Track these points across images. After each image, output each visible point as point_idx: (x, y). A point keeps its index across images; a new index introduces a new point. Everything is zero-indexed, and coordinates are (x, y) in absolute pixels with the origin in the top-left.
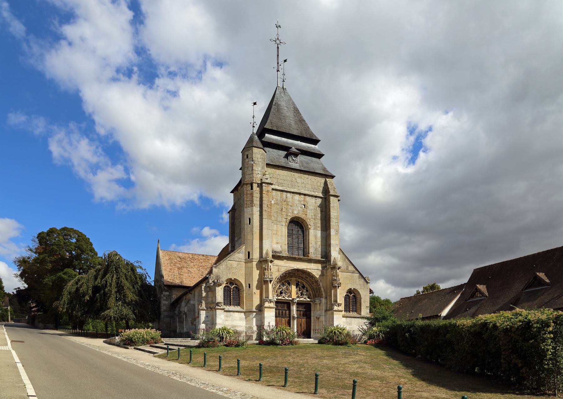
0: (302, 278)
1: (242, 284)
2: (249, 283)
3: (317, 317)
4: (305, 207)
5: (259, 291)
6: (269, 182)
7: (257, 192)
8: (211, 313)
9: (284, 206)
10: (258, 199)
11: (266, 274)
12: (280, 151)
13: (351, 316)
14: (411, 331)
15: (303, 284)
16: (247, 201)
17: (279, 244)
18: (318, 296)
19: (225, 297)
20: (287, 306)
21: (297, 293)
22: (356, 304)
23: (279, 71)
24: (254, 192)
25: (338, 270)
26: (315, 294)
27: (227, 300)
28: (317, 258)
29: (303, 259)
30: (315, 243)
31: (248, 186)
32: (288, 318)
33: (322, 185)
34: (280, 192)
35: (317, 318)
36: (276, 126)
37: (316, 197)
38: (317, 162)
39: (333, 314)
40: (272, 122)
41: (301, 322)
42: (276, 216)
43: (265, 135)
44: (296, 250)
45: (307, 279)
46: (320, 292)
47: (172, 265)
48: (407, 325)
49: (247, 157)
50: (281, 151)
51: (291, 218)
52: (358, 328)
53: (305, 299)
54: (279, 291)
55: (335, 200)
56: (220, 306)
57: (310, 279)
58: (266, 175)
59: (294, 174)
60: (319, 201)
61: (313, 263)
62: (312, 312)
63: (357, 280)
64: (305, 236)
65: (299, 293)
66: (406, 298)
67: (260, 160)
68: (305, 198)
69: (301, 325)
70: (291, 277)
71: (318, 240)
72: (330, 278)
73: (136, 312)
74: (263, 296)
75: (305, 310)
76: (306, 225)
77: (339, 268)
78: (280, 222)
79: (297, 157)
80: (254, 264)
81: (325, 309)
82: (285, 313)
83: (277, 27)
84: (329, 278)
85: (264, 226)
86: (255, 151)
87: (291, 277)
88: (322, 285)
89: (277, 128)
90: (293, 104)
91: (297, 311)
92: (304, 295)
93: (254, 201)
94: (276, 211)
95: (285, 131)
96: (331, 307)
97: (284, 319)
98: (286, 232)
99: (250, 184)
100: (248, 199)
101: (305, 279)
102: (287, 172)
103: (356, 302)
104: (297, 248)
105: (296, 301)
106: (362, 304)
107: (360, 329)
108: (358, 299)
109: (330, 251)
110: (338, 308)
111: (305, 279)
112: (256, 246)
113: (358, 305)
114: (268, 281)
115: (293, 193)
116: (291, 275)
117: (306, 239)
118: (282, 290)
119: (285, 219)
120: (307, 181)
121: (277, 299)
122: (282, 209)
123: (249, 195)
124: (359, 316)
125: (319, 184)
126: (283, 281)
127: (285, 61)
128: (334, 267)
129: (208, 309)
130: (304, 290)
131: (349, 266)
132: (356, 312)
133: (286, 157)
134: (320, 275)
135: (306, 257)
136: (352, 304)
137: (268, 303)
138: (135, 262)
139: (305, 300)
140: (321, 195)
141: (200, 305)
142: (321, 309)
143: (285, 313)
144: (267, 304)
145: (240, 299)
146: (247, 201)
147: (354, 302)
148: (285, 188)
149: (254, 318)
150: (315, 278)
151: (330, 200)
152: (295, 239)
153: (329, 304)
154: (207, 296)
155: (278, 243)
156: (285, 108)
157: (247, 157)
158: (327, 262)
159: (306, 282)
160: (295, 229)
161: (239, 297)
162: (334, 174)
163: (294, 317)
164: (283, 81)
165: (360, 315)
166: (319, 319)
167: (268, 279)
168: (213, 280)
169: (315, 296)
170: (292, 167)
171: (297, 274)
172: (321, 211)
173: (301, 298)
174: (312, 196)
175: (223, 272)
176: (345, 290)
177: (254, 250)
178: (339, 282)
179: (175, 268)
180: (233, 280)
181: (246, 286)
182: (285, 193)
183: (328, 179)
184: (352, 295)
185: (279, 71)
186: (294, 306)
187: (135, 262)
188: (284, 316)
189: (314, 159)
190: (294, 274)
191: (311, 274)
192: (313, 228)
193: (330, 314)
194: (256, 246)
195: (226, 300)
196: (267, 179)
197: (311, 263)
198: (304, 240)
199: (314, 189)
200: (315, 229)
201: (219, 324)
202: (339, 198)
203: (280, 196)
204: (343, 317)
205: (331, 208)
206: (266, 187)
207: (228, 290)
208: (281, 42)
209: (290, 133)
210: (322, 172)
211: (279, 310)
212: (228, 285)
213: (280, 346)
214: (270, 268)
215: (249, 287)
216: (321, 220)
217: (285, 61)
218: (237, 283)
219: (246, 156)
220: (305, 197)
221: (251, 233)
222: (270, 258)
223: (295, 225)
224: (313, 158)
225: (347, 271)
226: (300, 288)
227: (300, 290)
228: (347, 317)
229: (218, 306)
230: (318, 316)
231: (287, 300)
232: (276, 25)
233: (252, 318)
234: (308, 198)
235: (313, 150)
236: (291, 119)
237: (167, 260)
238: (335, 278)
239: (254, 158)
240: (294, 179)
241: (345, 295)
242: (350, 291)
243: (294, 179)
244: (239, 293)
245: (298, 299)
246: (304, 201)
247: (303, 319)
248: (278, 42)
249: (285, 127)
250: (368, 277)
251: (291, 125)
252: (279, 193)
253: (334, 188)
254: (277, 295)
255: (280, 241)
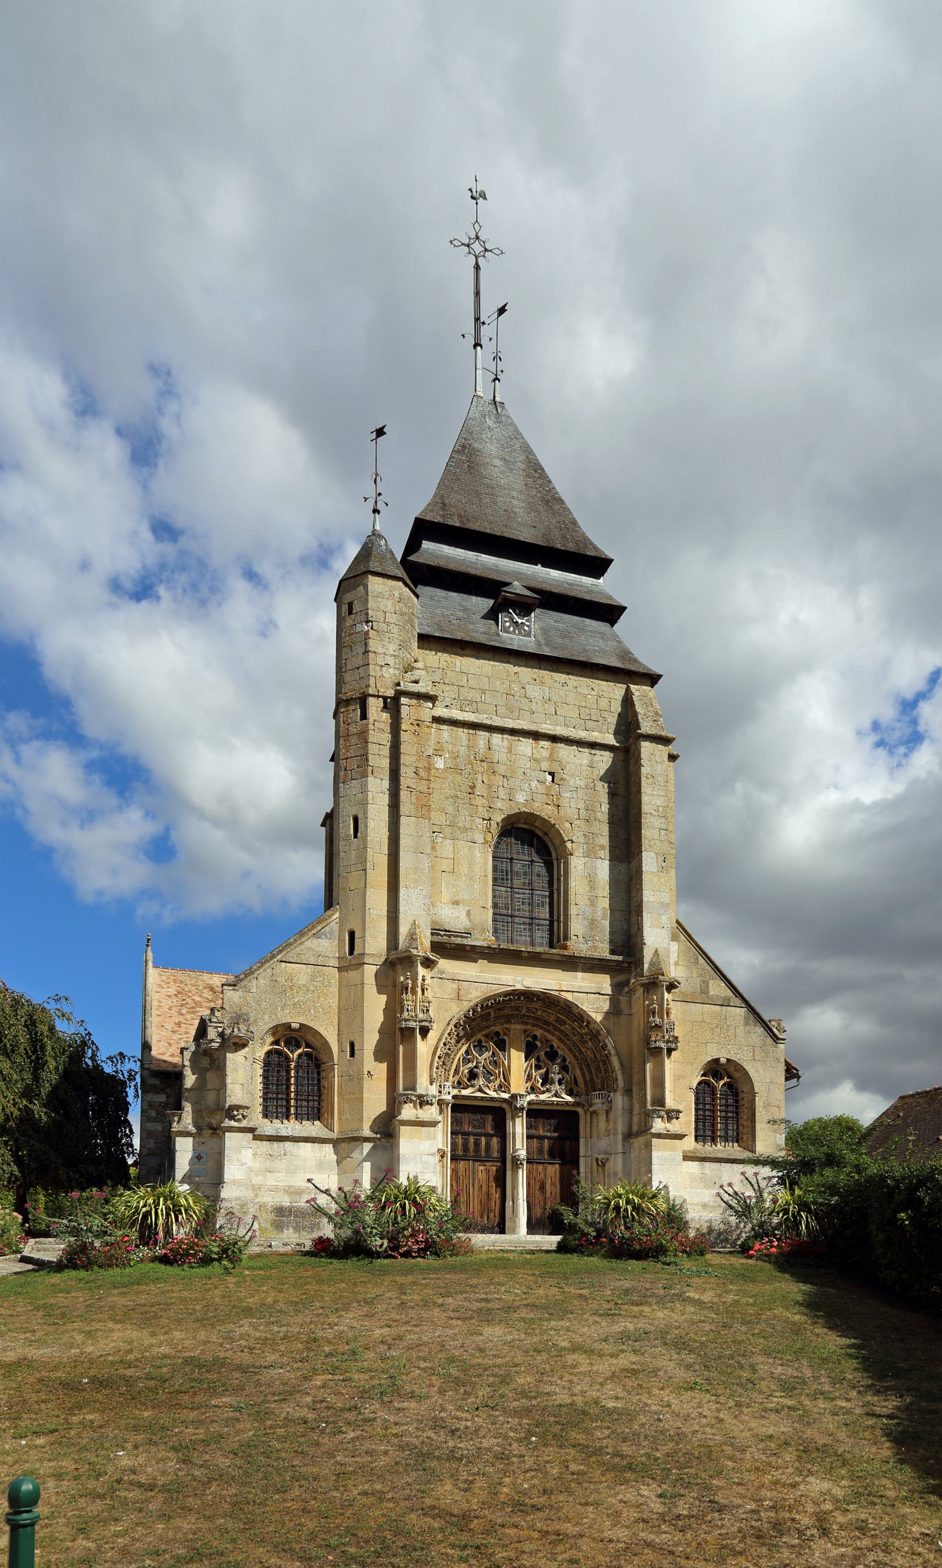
0: (547, 1023)
1: (326, 1043)
2: (352, 1038)
3: (597, 1159)
4: (553, 781)
5: (384, 1066)
6: (423, 690)
7: (382, 726)
8: (213, 1142)
9: (479, 776)
10: (386, 751)
11: (408, 1004)
12: (473, 597)
13: (720, 1155)
14: (921, 1201)
15: (552, 1047)
16: (346, 759)
17: (461, 905)
18: (603, 1085)
19: (267, 1088)
20: (493, 1120)
21: (529, 1078)
22: (737, 1113)
23: (481, 347)
24: (371, 727)
25: (669, 991)
26: (592, 1079)
27: (277, 1099)
28: (596, 955)
29: (544, 957)
30: (588, 903)
31: (352, 707)
32: (499, 1164)
33: (617, 707)
34: (466, 731)
35: (598, 1164)
36: (460, 516)
37: (593, 745)
38: (598, 633)
39: (648, 1146)
40: (446, 501)
41: (545, 1175)
42: (450, 809)
43: (421, 544)
44: (525, 929)
45: (563, 1028)
46: (606, 1071)
47: (184, 1011)
48: (903, 1178)
49: (350, 613)
50: (474, 599)
51: (503, 816)
52: (718, 1194)
53: (556, 1095)
54: (465, 1070)
55: (658, 753)
56: (239, 1120)
57: (573, 1028)
58: (415, 672)
59: (517, 669)
60: (604, 760)
61: (582, 971)
62: (582, 1141)
63: (741, 1031)
64: (555, 881)
65: (537, 1075)
66: (918, 1094)
67: (391, 618)
68: (552, 749)
69: (542, 1187)
70: (509, 1019)
71: (601, 893)
72: (642, 1023)
73: (23, 1156)
74: (398, 1082)
75: (556, 1134)
76: (557, 842)
77: (671, 987)
78: (465, 830)
79: (529, 614)
80: (370, 971)
81: (626, 1130)
82: (488, 1145)
83: (473, 197)
84: (638, 1021)
85: (401, 842)
86: (376, 586)
87: (509, 1022)
88: (616, 1048)
89: (461, 521)
90: (527, 450)
91: (528, 1137)
92: (552, 1083)
93: (370, 757)
94: (452, 793)
95: (488, 531)
96: (643, 1124)
97: (482, 1168)
98: (486, 863)
99: (358, 701)
100: (352, 753)
101: (555, 1028)
102: (492, 663)
103: (737, 1108)
104: (527, 921)
105: (523, 1102)
106: (757, 1113)
107: (726, 1197)
108: (743, 1095)
109: (640, 929)
110: (668, 1125)
111: (555, 1028)
112: (375, 912)
113: (745, 1117)
114: (413, 1029)
115: (513, 732)
116: (507, 1012)
117: (559, 890)
118: (476, 1067)
119: (484, 819)
120: (562, 693)
121: (454, 1097)
122: (473, 787)
123: (356, 737)
124: (746, 1155)
125: (604, 703)
126: (479, 1036)
127: (502, 311)
128: (653, 985)
129: (204, 1132)
130: (553, 1065)
131: (711, 983)
132: (737, 1142)
133: (492, 615)
134: (607, 1013)
135: (554, 951)
136: (723, 1114)
137: (415, 1107)
138: (48, 1001)
139: (555, 1099)
140: (610, 740)
141: (176, 1119)
142: (612, 1131)
143: (488, 1145)
144: (408, 1112)
145: (324, 1097)
146: (346, 759)
147: (730, 1109)
148: (485, 716)
149: (365, 1160)
150: (588, 1022)
151: (640, 753)
152: (521, 891)
153: (639, 1114)
154: (201, 1085)
155: (456, 903)
156: (497, 462)
157: (350, 613)
158: (633, 965)
159: (560, 1039)
160: (522, 857)
161: (319, 1090)
162: (656, 669)
163: (515, 1160)
164: (494, 380)
165: (753, 1151)
166: (604, 1165)
167: (412, 1024)
168: (220, 1030)
169: (591, 1086)
170: (509, 647)
171: (528, 1010)
172: (612, 795)
173: (544, 1092)
174: (580, 743)
175: (258, 1003)
176: (695, 1066)
177: (367, 924)
178: (671, 1034)
179: (193, 1019)
180: (294, 1030)
181: (341, 1051)
182: (483, 734)
183: (636, 687)
184: (722, 1083)
185: (481, 347)
186: (518, 1121)
187: (48, 1001)
188: (483, 1154)
189: (592, 624)
190: (517, 1009)
191: (575, 1010)
192: (581, 850)
193: (640, 1149)
194: (375, 912)
195: (274, 1099)
196: (416, 682)
197: (576, 971)
198: (551, 893)
199: (587, 721)
200: (590, 854)
201: (234, 1182)
202: (671, 748)
203: (465, 743)
204: (687, 1158)
205: (643, 779)
206: (413, 710)
207: (279, 1065)
208: (486, 250)
209: (506, 535)
210: (615, 662)
211: (464, 1134)
212: (282, 1047)
213: (386, 1261)
214: (422, 985)
215: (352, 1054)
216: (611, 823)
217: (502, 311)
218: (313, 1039)
219: (345, 608)
220: (555, 745)
221: (360, 867)
222: (423, 947)
223: (523, 844)
224: (588, 621)
225: (702, 997)
226: (538, 1059)
227: (538, 1067)
228: (703, 1159)
229: (232, 1118)
230: (600, 1157)
231: (492, 1099)
232: (471, 190)
233: (360, 1160)
234: (564, 751)
235: (585, 592)
236: (515, 494)
237: (169, 996)
238: (658, 1020)
239: (370, 612)
240: (516, 687)
241: (699, 1084)
242: (714, 1069)
243: (516, 687)
244: (319, 1073)
245: (532, 1097)
246: (552, 758)
247: (550, 1168)
248: (477, 247)
249: (491, 518)
250: (779, 1021)
251: (515, 513)
252: (462, 733)
253: (657, 714)
254: (459, 1083)
255: (463, 895)
